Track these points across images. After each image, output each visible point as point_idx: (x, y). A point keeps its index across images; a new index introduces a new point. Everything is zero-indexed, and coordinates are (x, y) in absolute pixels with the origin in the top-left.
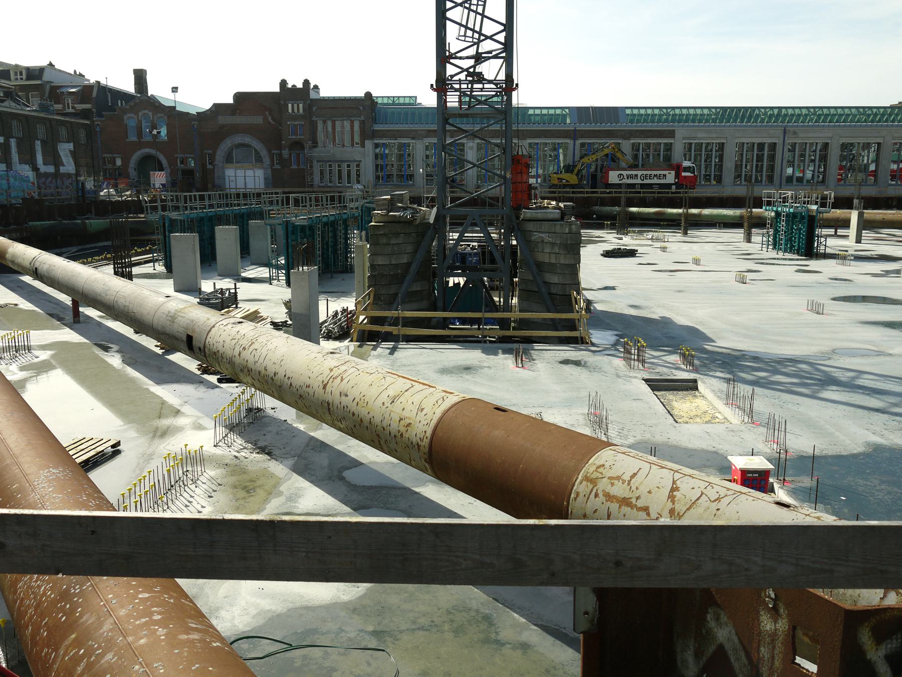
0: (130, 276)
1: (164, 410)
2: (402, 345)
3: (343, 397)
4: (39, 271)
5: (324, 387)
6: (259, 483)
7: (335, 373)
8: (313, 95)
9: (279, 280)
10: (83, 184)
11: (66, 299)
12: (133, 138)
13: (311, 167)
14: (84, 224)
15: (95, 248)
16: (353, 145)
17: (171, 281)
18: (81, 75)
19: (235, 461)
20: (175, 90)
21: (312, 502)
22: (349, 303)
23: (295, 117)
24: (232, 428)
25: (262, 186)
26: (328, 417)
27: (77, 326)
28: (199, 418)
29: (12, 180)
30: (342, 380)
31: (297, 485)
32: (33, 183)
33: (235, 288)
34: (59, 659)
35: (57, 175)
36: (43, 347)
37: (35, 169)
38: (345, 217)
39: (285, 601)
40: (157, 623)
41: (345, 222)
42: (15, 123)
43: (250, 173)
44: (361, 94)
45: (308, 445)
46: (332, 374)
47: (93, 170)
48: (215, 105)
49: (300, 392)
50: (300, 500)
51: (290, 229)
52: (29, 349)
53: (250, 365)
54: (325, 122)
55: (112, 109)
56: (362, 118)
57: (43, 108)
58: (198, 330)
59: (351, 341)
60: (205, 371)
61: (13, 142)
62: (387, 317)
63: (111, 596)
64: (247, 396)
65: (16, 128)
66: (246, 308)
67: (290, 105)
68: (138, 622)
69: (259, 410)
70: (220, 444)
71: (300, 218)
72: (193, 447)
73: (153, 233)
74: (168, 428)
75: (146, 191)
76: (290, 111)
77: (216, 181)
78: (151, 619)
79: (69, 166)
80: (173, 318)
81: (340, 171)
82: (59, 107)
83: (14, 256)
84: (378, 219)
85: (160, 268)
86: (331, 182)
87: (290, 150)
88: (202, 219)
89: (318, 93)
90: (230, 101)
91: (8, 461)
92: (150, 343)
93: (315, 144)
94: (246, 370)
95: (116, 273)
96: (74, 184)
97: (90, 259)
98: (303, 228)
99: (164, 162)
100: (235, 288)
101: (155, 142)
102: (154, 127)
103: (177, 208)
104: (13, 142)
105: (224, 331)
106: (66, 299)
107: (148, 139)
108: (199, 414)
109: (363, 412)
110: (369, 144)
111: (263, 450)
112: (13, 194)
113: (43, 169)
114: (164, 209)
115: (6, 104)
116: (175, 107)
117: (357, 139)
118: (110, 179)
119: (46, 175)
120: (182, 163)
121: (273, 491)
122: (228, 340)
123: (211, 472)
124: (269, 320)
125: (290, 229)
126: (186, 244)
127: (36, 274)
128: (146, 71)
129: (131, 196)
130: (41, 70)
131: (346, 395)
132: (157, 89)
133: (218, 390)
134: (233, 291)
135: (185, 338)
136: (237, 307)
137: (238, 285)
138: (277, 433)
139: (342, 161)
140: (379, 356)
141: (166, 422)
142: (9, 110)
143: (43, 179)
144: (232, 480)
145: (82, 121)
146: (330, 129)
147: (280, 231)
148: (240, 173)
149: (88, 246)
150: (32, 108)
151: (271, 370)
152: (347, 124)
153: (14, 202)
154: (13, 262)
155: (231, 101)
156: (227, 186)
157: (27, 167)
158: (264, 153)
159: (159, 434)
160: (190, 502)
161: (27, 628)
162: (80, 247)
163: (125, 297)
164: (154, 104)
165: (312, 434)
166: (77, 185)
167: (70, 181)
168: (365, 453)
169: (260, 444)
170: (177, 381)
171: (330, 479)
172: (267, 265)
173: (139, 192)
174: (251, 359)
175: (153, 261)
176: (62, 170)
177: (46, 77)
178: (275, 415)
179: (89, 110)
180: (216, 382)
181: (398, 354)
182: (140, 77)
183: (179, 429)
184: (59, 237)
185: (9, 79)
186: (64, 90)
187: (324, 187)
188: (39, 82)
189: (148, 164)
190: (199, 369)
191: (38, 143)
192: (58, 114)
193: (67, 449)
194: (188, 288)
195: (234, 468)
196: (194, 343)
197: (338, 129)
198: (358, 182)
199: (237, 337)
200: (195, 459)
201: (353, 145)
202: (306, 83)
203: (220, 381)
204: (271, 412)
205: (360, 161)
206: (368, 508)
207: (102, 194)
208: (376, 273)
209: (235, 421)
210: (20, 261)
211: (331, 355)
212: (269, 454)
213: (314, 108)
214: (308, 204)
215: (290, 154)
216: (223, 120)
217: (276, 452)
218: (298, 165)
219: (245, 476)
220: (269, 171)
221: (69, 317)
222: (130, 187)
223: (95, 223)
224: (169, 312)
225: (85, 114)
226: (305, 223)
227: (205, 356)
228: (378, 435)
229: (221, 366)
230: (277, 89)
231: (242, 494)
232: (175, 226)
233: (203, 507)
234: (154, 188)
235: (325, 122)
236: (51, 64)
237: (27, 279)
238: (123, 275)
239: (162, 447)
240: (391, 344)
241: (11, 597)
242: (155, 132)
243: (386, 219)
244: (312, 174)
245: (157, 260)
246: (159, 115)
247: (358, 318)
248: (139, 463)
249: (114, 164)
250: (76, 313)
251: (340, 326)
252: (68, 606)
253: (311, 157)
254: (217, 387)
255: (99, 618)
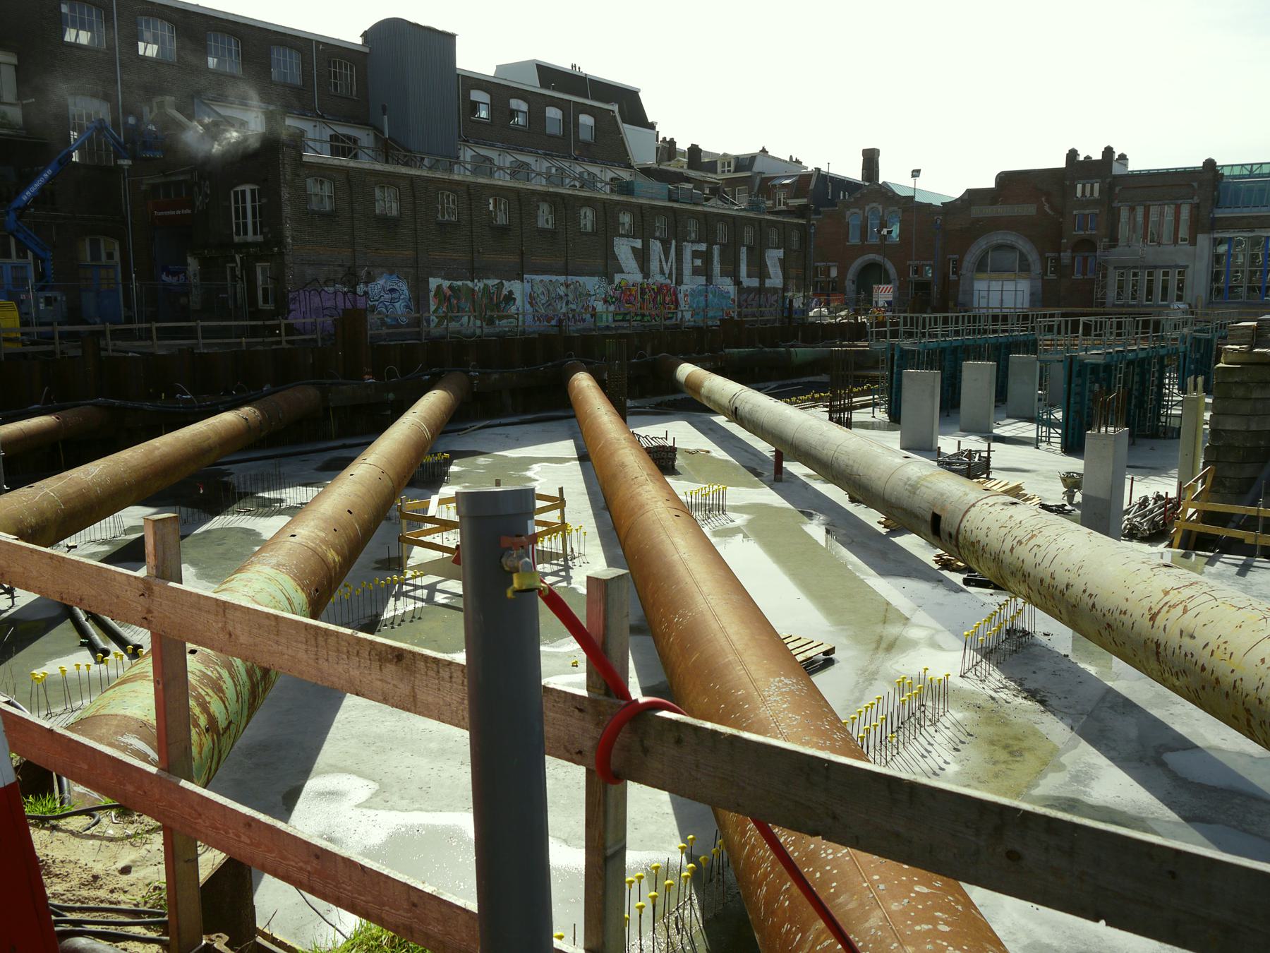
0: (848, 424)
1: (887, 613)
2: (1259, 562)
3: (1186, 640)
4: (739, 412)
5: (1153, 618)
6: (1025, 744)
7: (1173, 598)
8: (1117, 169)
9: (1049, 443)
10: (791, 301)
11: (766, 449)
12: (854, 240)
13: (1105, 276)
14: (789, 353)
15: (798, 384)
16: (1175, 242)
17: (897, 434)
18: (798, 161)
19: (991, 705)
20: (916, 173)
21: (1111, 790)
22: (1168, 487)
23: (1085, 203)
24: (988, 653)
25: (1026, 305)
26: (1153, 665)
27: (779, 485)
28: (937, 631)
29: (710, 296)
30: (1185, 611)
31: (1087, 759)
32: (733, 301)
33: (989, 451)
34: (808, 946)
35: (761, 290)
36: (737, 509)
37: (738, 283)
38: (1163, 352)
39: (1072, 937)
40: (943, 936)
41: (1162, 358)
42: (720, 226)
43: (1009, 286)
44: (1198, 163)
45: (1103, 699)
46: (1167, 599)
47: (803, 285)
48: (969, 192)
49: (1109, 617)
50: (1093, 784)
51: (1076, 368)
52: (722, 509)
53: (1028, 567)
54: (1132, 209)
55: (832, 203)
56: (1196, 200)
57: (753, 206)
58: (949, 507)
59: (1170, 546)
60: (946, 565)
61: (716, 248)
62: (1233, 515)
63: (876, 877)
64: (1008, 612)
65: (721, 231)
66: (1001, 480)
67: (1079, 187)
68: (918, 928)
69: (1025, 633)
70: (969, 674)
71: (1093, 353)
72: (937, 673)
73: (875, 367)
74: (896, 639)
75: (866, 312)
76: (1079, 194)
77: (961, 297)
78: (935, 929)
79: (775, 279)
80: (914, 488)
81: (1150, 282)
82: (769, 203)
83: (710, 391)
84: (1231, 358)
85: (881, 415)
86: (1134, 298)
87: (1073, 251)
88: (943, 350)
89: (1126, 165)
90: (991, 184)
91: (731, 657)
92: (872, 518)
93: (1114, 241)
94: (1019, 575)
95: (831, 419)
96: (780, 301)
97: (794, 399)
98: (1095, 368)
99: (892, 271)
100: (989, 451)
101: (883, 246)
102: (883, 225)
103: (910, 335)
104: (716, 248)
105: (985, 512)
106: (766, 449)
107: (874, 240)
108: (939, 627)
109: (1222, 667)
110: (1203, 240)
111: (1032, 695)
112: (710, 314)
113: (747, 282)
114: (895, 334)
115: (712, 202)
116: (913, 197)
117: (1183, 232)
118: (821, 295)
119: (750, 290)
120: (916, 272)
121: (1050, 761)
122: (995, 527)
123: (956, 715)
124: (1036, 501)
125: (1076, 368)
126: (922, 386)
127: (735, 414)
128: (878, 151)
129: (847, 317)
130: (752, 158)
131: (1192, 637)
132: (892, 174)
133: (962, 595)
134: (985, 454)
135: (929, 517)
136: (988, 478)
137: (994, 446)
138: (1054, 674)
139: (1156, 267)
140: (1219, 576)
141: (893, 630)
142: (716, 210)
143: (745, 296)
144: (990, 731)
145: (796, 221)
146: (1140, 219)
147: (1058, 373)
148: (996, 286)
149: (789, 382)
150: (739, 206)
151: (1062, 579)
152: (1169, 210)
153: (710, 323)
154: (708, 398)
155: (992, 185)
156: (976, 305)
157: (728, 280)
158: (1033, 257)
159: (884, 645)
160: (929, 752)
161: (760, 886)
162: (780, 383)
163: (848, 454)
164: (886, 195)
165: (1110, 684)
166: (784, 302)
167: (775, 297)
168: (1202, 731)
169: (1030, 685)
170: (907, 575)
171: (1141, 760)
172: (1030, 420)
173: (857, 313)
174: (1029, 559)
175: (874, 405)
176: (768, 283)
177: (757, 167)
178: (1050, 645)
179: (806, 206)
180: (960, 583)
181: (1252, 576)
182: (871, 159)
183: (912, 644)
184: (757, 370)
185: (716, 173)
186: (776, 182)
187: (1123, 306)
188: (748, 174)
189: (870, 275)
190: (937, 562)
191: (744, 250)
192: (770, 213)
193: (794, 653)
194: (921, 445)
195: (990, 712)
196: (942, 525)
197: (1153, 218)
198: (1180, 298)
199: (1010, 524)
200: (940, 691)
201: (1175, 242)
202: (1108, 151)
203: (966, 582)
204: (1044, 640)
205: (1187, 267)
206: (1209, 822)
207: (811, 314)
208: (1220, 443)
209: (992, 644)
210: (717, 397)
211: (1165, 569)
212: (1042, 702)
213: (1117, 189)
214: (1108, 330)
215: (1073, 258)
216: (977, 211)
217: (1053, 702)
218: (1084, 274)
219: (1006, 729)
220: (1039, 283)
221: (769, 472)
222: (845, 305)
223: (802, 352)
224: (909, 479)
225: (801, 212)
226: (1100, 360)
227: (957, 546)
228: (1248, 711)
229: (970, 559)
230: (1061, 164)
231: (1002, 755)
232: (908, 359)
233: (945, 762)
234: (877, 307)
235: (1132, 209)
236: (764, 151)
237: (721, 420)
238: (839, 422)
239: (888, 664)
240: (1240, 559)
241: (737, 838)
242: (885, 231)
243: (1245, 358)
244: (1104, 287)
245: (878, 404)
246: (891, 209)
247: (1185, 511)
248: (858, 683)
249: (828, 275)
250: (779, 469)
251: (1153, 523)
252: (818, 875)
253: (1106, 261)
254: (962, 590)
255: (862, 905)
